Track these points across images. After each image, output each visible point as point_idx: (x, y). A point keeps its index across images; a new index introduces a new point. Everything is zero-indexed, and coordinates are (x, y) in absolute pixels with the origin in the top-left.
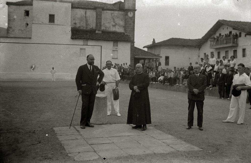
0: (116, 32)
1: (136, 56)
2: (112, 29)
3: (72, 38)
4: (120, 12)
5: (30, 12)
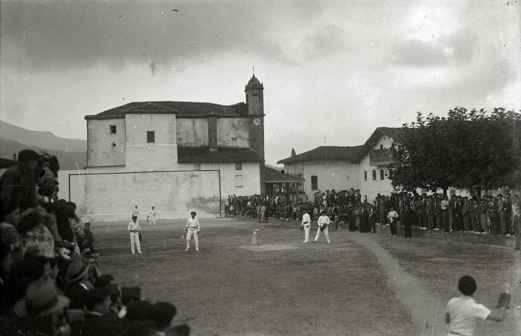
2: (231, 144)
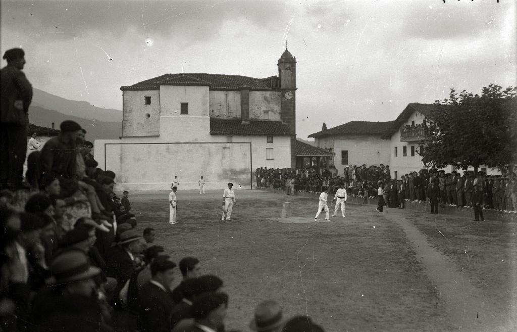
2: (263, 117)
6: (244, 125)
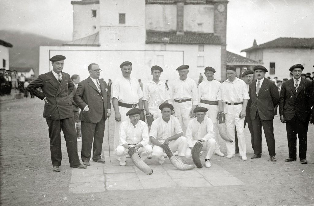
0: (202, 32)
1: (228, 63)
3: (147, 43)
4: (208, 6)
5: (97, 12)
6: (179, 36)
